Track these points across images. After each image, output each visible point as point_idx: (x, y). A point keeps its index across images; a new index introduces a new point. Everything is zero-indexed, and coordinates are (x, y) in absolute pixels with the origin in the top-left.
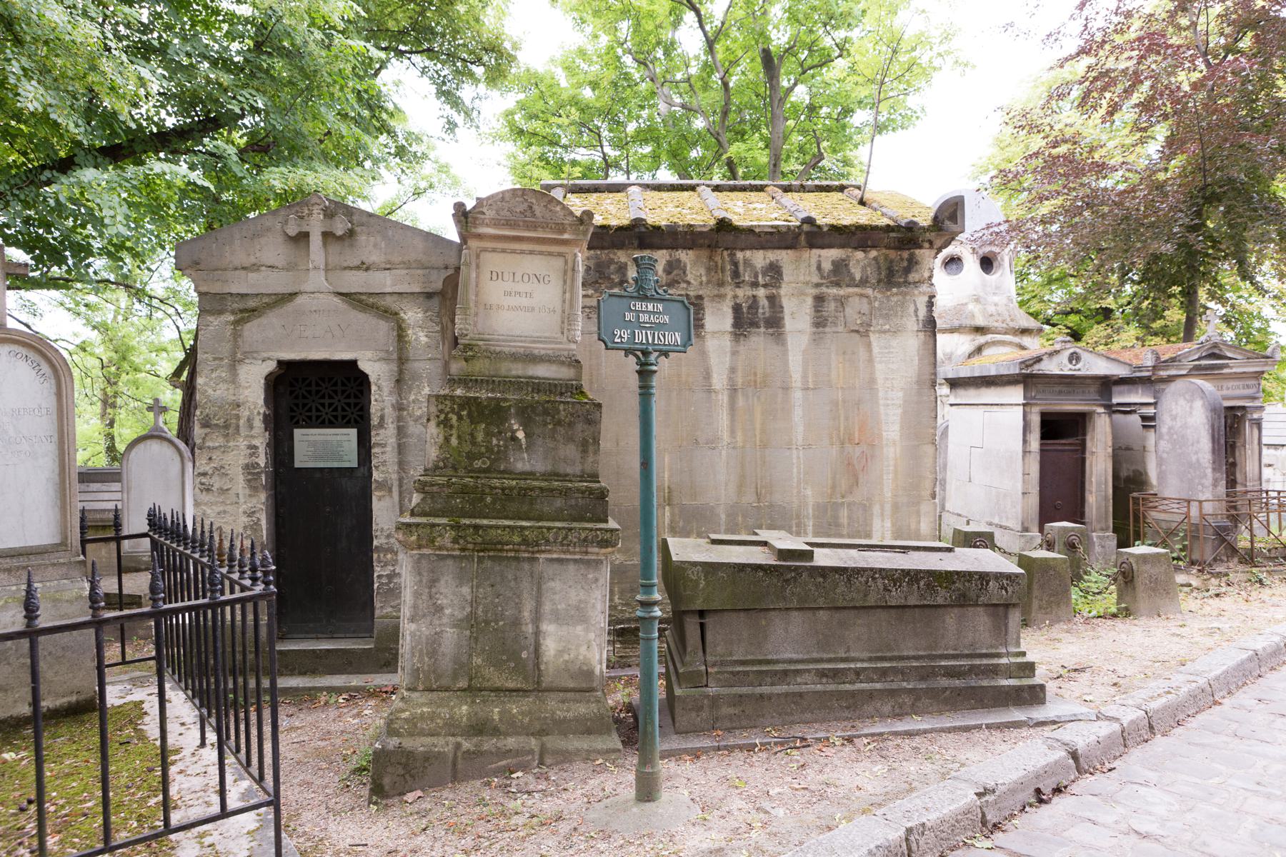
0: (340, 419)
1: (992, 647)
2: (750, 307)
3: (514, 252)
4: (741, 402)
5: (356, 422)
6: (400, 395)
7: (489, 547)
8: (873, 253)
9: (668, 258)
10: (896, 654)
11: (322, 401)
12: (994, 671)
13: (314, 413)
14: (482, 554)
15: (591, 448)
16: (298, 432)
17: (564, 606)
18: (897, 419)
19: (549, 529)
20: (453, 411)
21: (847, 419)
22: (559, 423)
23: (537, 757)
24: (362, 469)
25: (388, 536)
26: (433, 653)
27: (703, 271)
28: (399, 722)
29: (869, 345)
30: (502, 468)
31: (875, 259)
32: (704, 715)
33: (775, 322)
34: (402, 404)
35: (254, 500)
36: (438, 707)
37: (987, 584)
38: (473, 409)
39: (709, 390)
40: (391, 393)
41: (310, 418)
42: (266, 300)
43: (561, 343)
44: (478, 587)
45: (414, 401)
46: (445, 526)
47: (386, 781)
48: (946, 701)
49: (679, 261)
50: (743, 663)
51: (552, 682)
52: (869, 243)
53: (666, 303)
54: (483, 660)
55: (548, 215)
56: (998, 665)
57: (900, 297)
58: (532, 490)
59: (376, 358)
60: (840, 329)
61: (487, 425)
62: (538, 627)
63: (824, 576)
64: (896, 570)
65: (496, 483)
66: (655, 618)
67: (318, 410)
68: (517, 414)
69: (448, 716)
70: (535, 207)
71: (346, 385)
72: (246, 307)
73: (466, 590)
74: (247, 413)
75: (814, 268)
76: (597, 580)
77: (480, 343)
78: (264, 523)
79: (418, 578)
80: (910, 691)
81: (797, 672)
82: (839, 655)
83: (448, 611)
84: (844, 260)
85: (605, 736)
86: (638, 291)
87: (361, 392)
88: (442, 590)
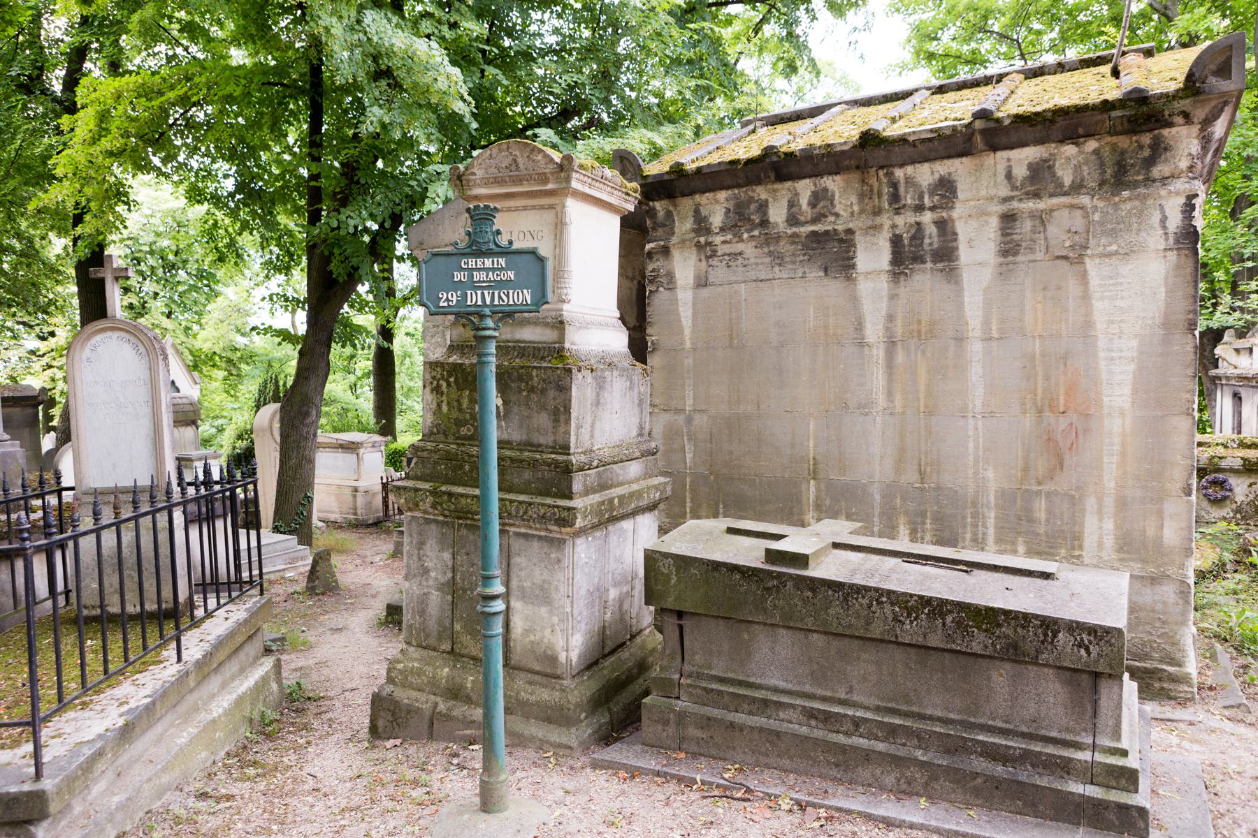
1: (1068, 730)
2: (913, 238)
4: (900, 357)
8: (1092, 145)
9: (813, 188)
10: (915, 709)
12: (1065, 768)
15: (562, 418)
17: (529, 584)
18: (1128, 378)
19: (511, 501)
20: (443, 378)
21: (1047, 378)
22: (532, 390)
27: (854, 199)
29: (1084, 276)
31: (1096, 152)
32: (671, 730)
33: (946, 255)
37: (1055, 635)
38: (459, 375)
39: (862, 344)
47: (381, 723)
48: (977, 792)
49: (825, 190)
50: (722, 680)
52: (1081, 131)
53: (509, 256)
56: (1071, 760)
57: (1137, 203)
60: (1039, 255)
63: (813, 590)
64: (911, 595)
70: (519, 160)
73: (447, 556)
80: (923, 765)
81: (780, 705)
82: (837, 695)
83: (433, 574)
84: (1046, 161)
85: (564, 729)
88: (428, 553)
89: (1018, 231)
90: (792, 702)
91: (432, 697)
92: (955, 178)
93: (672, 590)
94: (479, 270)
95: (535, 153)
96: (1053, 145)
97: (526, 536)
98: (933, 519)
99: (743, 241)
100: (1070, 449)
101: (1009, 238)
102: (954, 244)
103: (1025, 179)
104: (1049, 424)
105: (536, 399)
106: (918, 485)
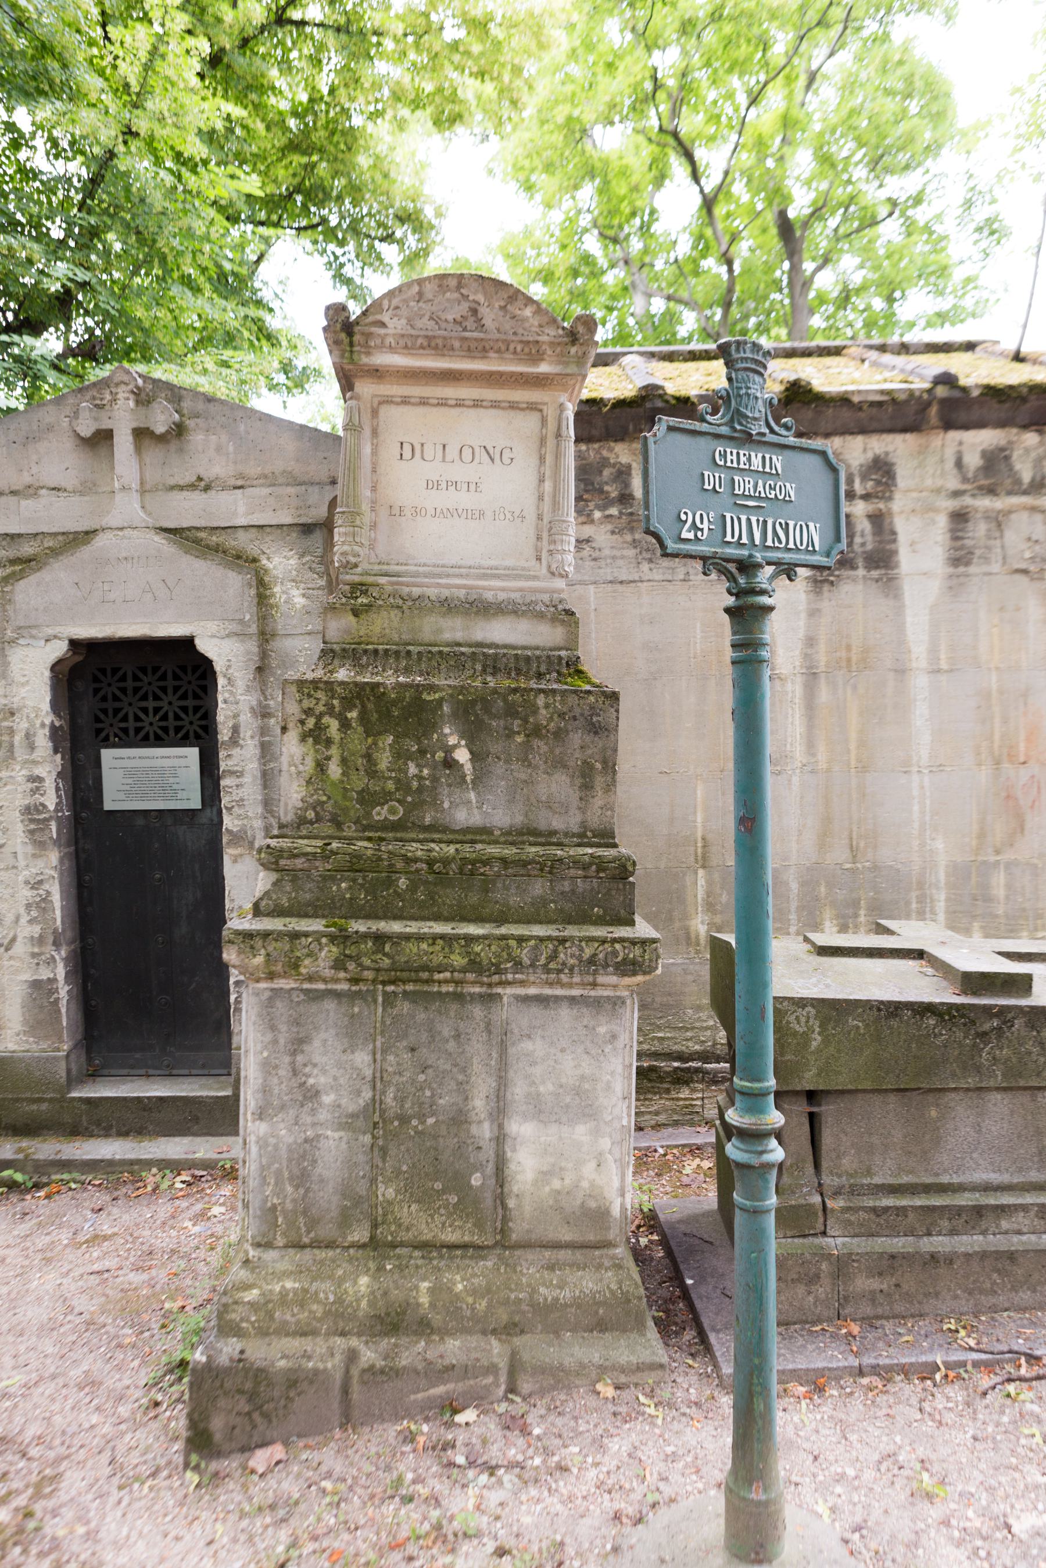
0: (172, 732)
3: (443, 403)
4: (824, 695)
5: (198, 737)
6: (263, 692)
7: (405, 975)
11: (144, 704)
13: (131, 724)
14: (390, 988)
15: (599, 781)
16: (108, 755)
17: (550, 1087)
19: (521, 940)
20: (330, 711)
21: (1005, 721)
22: (536, 732)
23: (503, 1379)
24: (208, 811)
26: (302, 1179)
28: (240, 1309)
30: (428, 820)
32: (822, 1290)
34: (267, 706)
35: (40, 863)
36: (314, 1279)
38: (370, 706)
40: (248, 690)
41: (125, 731)
42: (49, 543)
43: (535, 578)
44: (384, 1051)
46: (318, 936)
47: (217, 1424)
51: (529, 1231)
53: (788, 453)
54: (398, 1192)
55: (508, 325)
58: (486, 863)
59: (223, 633)
60: (996, 567)
61: (397, 737)
62: (501, 1127)
65: (415, 849)
66: (767, 1166)
67: (137, 719)
68: (455, 714)
69: (332, 1298)
70: (483, 311)
71: (180, 679)
72: (19, 554)
73: (362, 1058)
74: (24, 725)
75: (950, 464)
76: (614, 1037)
77: (382, 580)
78: (56, 898)
79: (269, 1036)
81: (1002, 1210)
83: (327, 1099)
84: (1002, 449)
85: (634, 1335)
87: (204, 689)
88: (317, 1058)
89: (970, 534)
90: (1020, 1201)
91: (338, 1340)
92: (894, 460)
93: (812, 1058)
95: (520, 303)
96: (1015, 430)
97: (542, 1000)
98: (868, 909)
99: (592, 522)
100: (1032, 807)
101: (959, 543)
102: (893, 546)
103: (978, 469)
104: (1008, 778)
105: (544, 748)
106: (848, 866)
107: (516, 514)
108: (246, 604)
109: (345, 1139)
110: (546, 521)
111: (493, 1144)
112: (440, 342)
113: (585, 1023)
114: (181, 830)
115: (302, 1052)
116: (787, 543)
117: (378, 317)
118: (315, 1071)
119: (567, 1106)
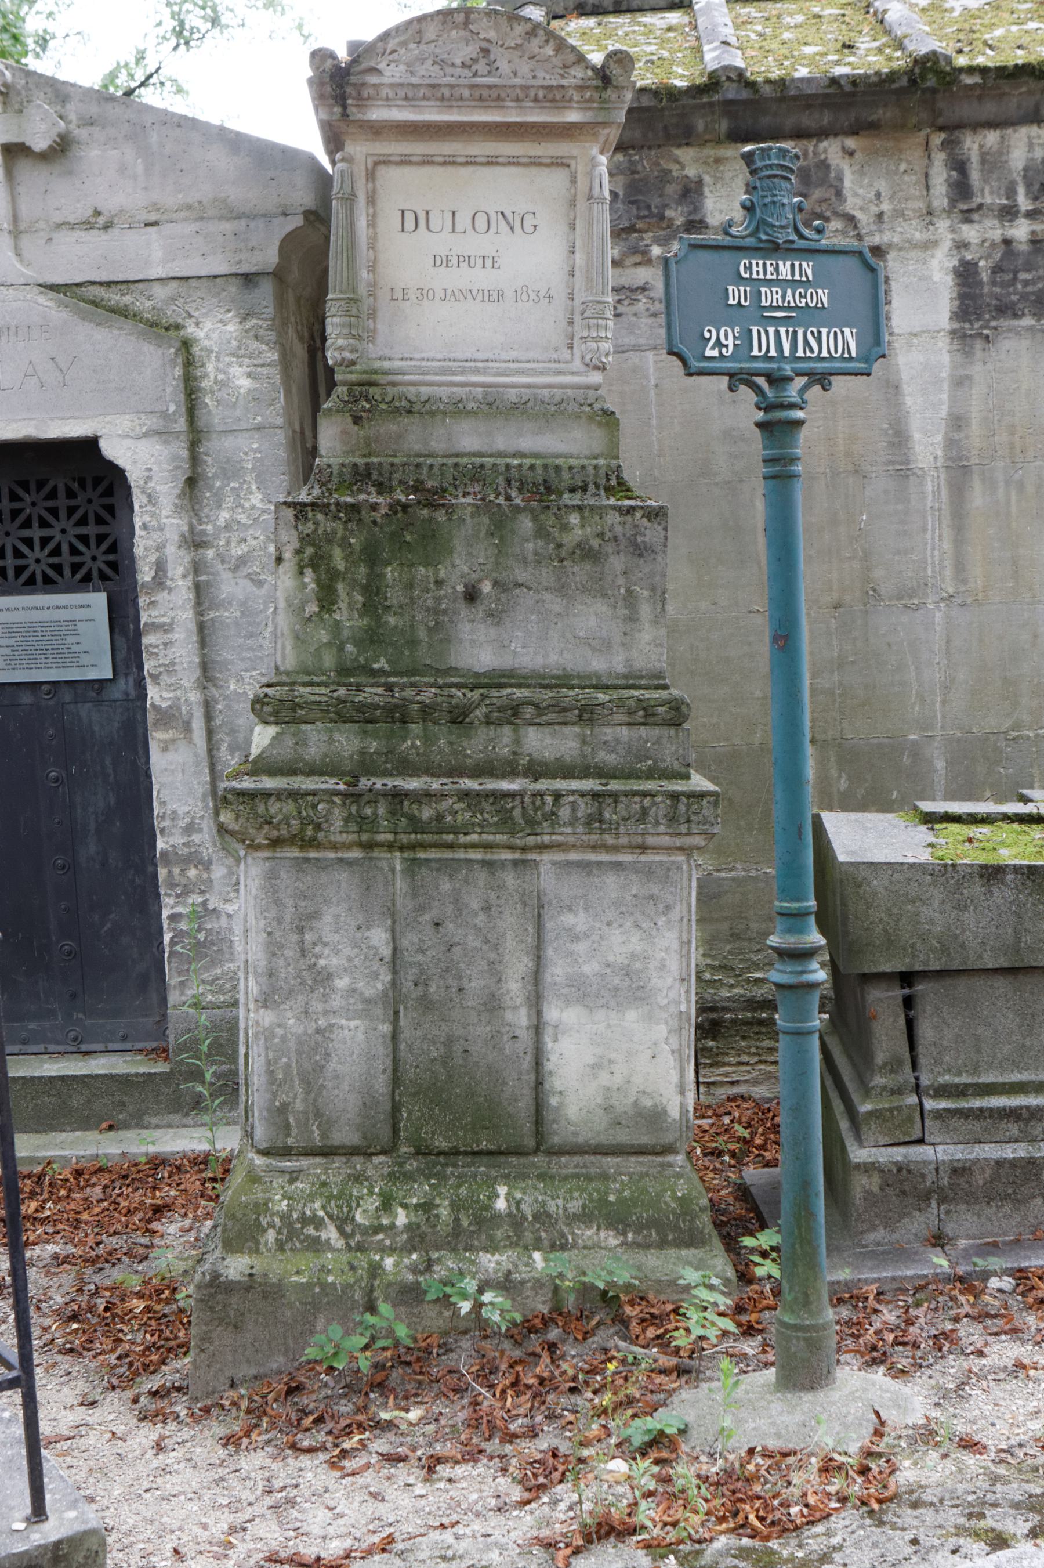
0: (67, 571)
3: (449, 162)
4: (977, 498)
5: (104, 577)
11: (26, 533)
24: (122, 681)
25: (190, 829)
34: (203, 532)
45: (227, 527)
53: (823, 259)
62: (539, 1013)
73: (379, 937)
79: (273, 913)
83: (342, 983)
86: (754, 233)
87: (111, 509)
88: (329, 937)
94: (769, 283)
107: (542, 294)
108: (169, 390)
109: (362, 1028)
110: (577, 301)
111: (532, 1032)
112: (447, 92)
113: (634, 892)
114: (84, 710)
115: (311, 929)
116: (820, 351)
117: (372, 64)
118: (327, 951)
119: (617, 989)
